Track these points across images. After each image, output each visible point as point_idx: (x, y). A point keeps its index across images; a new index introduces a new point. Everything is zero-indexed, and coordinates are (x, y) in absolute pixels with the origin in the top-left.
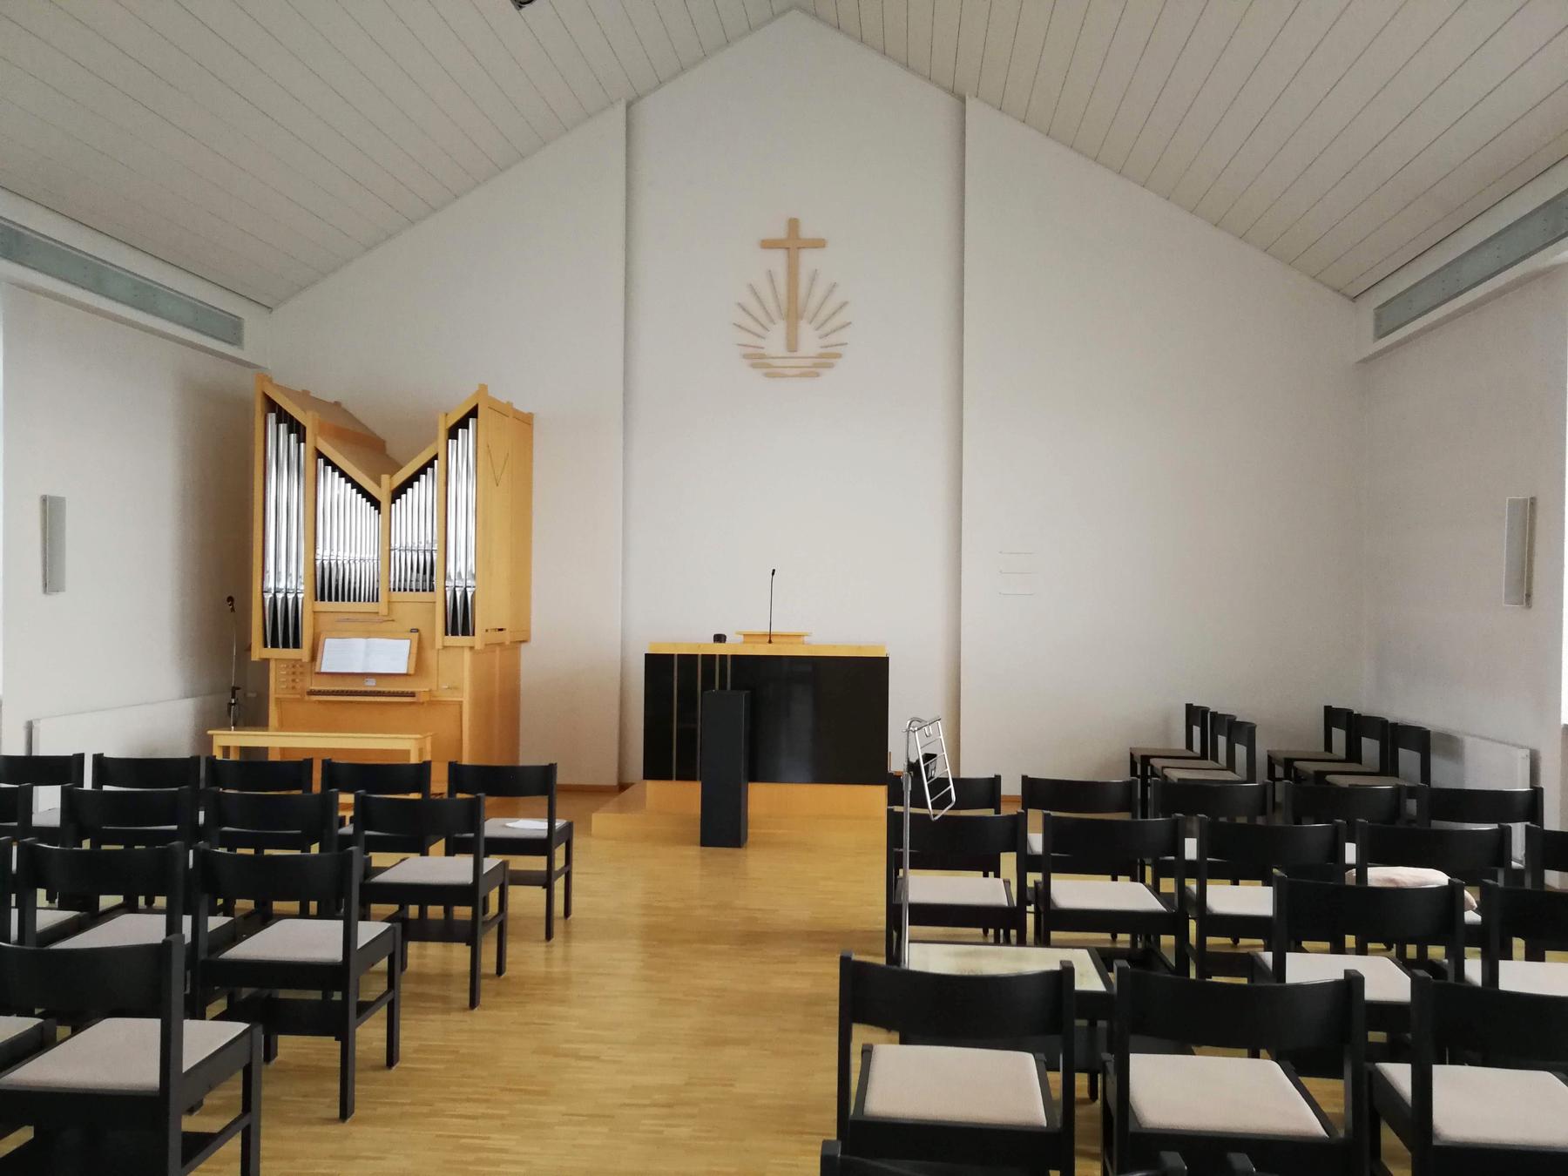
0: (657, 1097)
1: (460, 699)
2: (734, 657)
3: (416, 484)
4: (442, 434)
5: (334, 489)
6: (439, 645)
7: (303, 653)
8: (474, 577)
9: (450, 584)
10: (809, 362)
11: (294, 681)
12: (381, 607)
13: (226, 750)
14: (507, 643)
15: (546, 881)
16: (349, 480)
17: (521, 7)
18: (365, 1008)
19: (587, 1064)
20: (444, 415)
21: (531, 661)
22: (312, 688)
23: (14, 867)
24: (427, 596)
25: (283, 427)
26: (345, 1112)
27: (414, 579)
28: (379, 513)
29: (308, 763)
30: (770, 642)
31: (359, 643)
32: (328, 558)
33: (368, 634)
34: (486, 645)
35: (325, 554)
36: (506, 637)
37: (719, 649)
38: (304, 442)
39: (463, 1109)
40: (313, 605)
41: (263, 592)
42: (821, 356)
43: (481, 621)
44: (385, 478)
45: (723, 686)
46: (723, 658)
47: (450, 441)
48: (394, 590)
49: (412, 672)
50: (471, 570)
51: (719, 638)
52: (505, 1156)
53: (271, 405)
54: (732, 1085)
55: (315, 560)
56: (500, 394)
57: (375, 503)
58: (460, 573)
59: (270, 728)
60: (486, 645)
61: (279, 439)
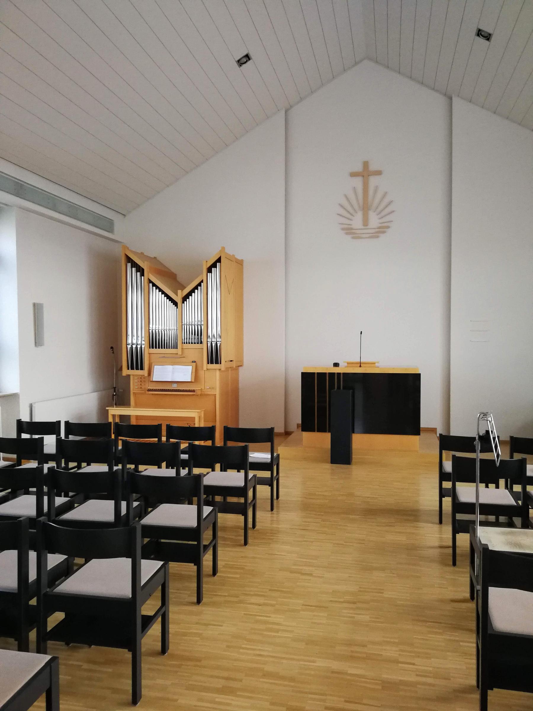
0: (348, 598)
1: (215, 393)
2: (344, 374)
3: (193, 294)
4: (205, 271)
5: (156, 297)
6: (205, 369)
7: (145, 372)
8: (220, 337)
9: (209, 340)
10: (373, 231)
11: (141, 385)
12: (179, 351)
13: (114, 416)
14: (234, 367)
15: (269, 482)
16: (163, 293)
17: (241, 66)
18: (206, 547)
19: (304, 577)
20: (206, 261)
21: (244, 375)
22: (149, 388)
23: (162, 541)
24: (199, 346)
25: (134, 269)
26: (199, 601)
27: (193, 338)
28: (177, 308)
29: (159, 426)
30: (360, 366)
31: (170, 368)
32: (155, 329)
33: (173, 364)
34: (226, 368)
35: (162, 328)
36: (234, 364)
37: (336, 370)
38: (144, 276)
39: (254, 600)
40: (149, 350)
41: (127, 345)
42: (379, 228)
43: (224, 356)
44: (179, 292)
45: (339, 388)
46: (339, 374)
47: (208, 273)
48: (184, 343)
49: (193, 381)
50: (219, 334)
51: (336, 365)
52: (281, 628)
53: (129, 260)
54: (382, 593)
55: (149, 330)
56: (229, 251)
57: (175, 304)
58: (214, 335)
59: (131, 407)
60: (226, 368)
61: (132, 274)
